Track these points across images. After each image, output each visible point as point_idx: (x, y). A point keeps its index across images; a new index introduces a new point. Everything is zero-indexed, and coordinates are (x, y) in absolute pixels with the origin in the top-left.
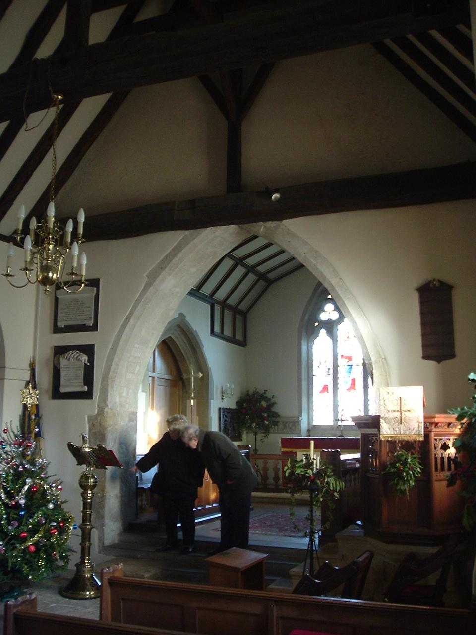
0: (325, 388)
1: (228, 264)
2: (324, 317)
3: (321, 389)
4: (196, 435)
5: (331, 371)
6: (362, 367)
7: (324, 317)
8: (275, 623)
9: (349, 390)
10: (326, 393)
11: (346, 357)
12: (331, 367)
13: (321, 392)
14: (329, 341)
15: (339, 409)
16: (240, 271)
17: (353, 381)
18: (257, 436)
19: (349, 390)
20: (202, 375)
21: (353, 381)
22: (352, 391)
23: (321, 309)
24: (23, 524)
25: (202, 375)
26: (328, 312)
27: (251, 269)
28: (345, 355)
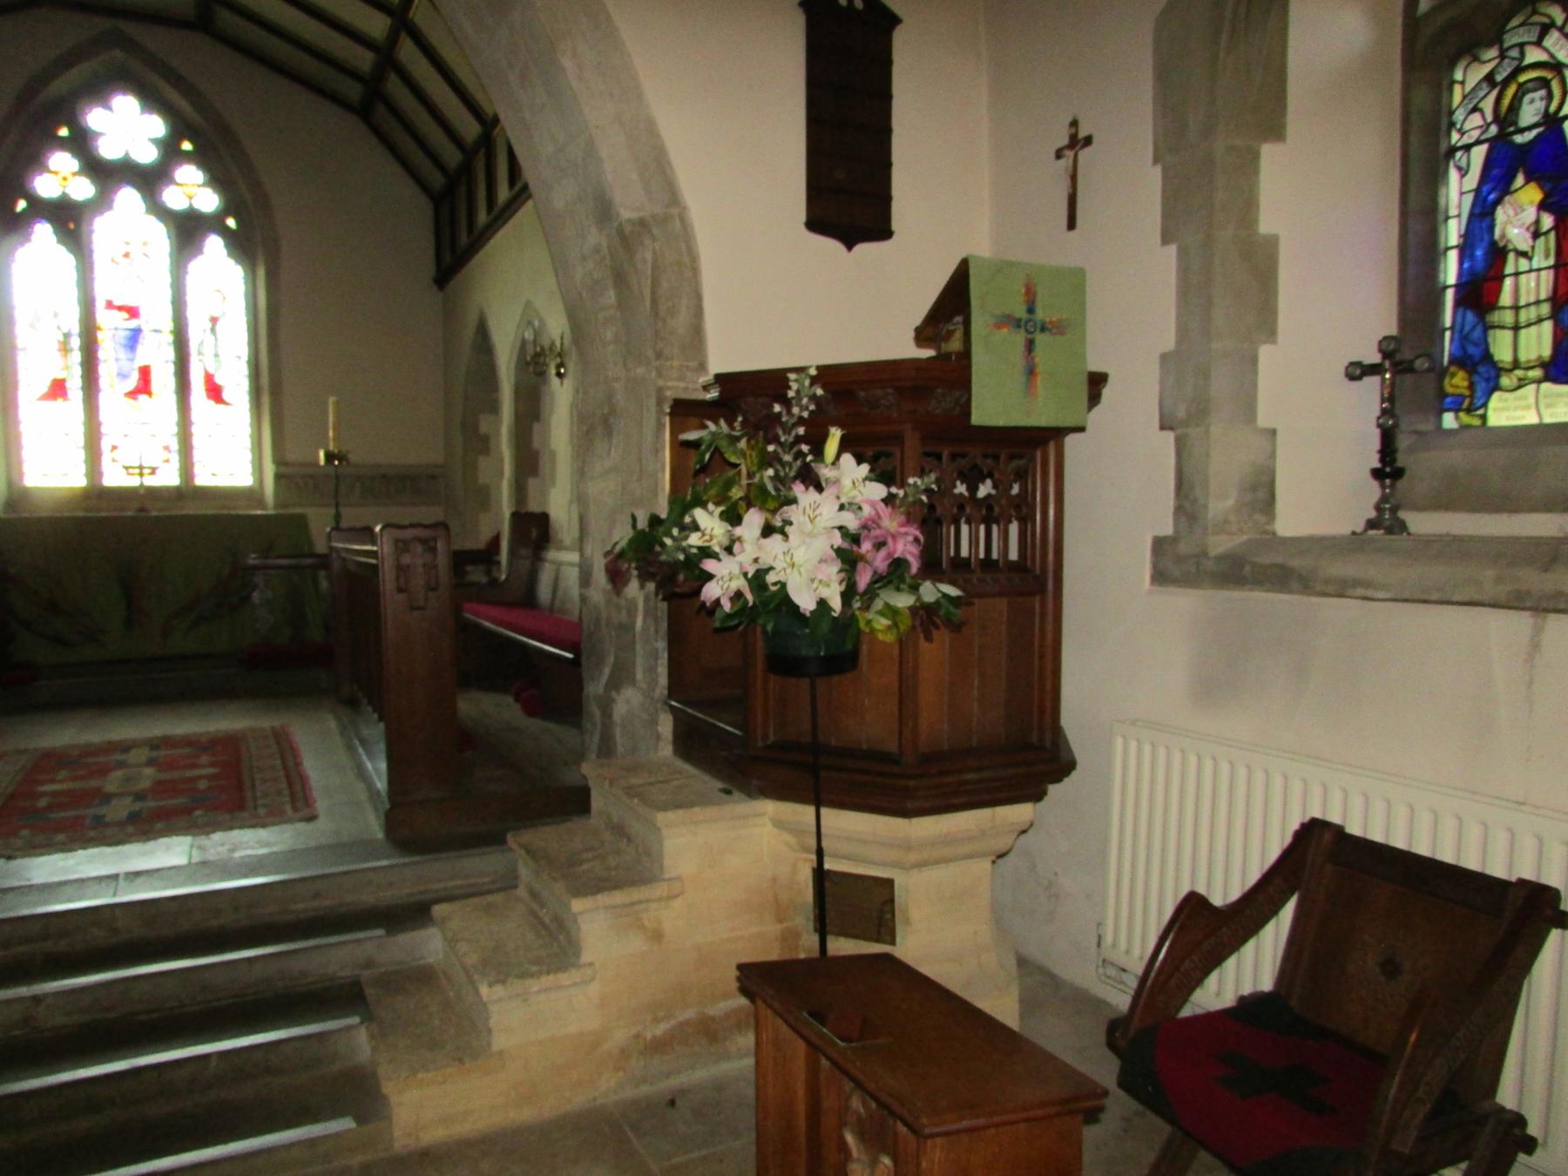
0: (58, 389)
1: (470, 129)
2: (46, 186)
3: (45, 387)
4: (788, 564)
5: (76, 342)
6: (171, 338)
7: (46, 186)
8: (1037, 630)
9: (133, 394)
10: (60, 400)
11: (120, 308)
12: (75, 328)
13: (39, 399)
14: (66, 259)
15: (105, 445)
16: (453, 157)
17: (145, 372)
18: (609, 548)
19: (133, 394)
20: (956, 491)
21: (145, 372)
22: (143, 397)
23: (34, 161)
24: (1476, 422)
25: (956, 491)
26: (60, 176)
27: (466, 168)
28: (117, 303)
